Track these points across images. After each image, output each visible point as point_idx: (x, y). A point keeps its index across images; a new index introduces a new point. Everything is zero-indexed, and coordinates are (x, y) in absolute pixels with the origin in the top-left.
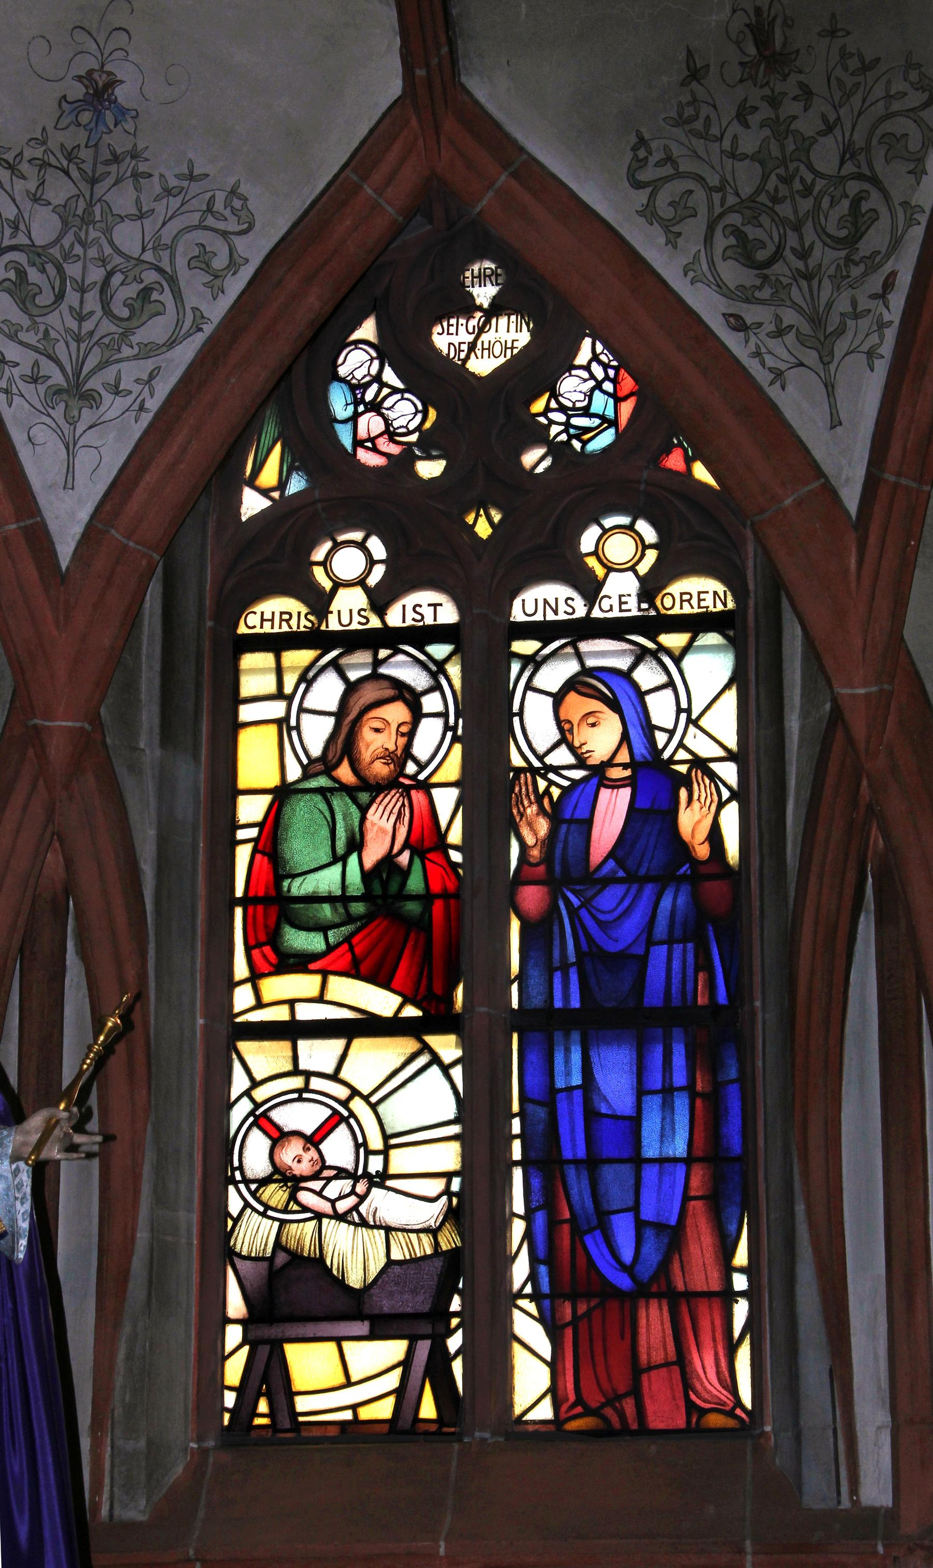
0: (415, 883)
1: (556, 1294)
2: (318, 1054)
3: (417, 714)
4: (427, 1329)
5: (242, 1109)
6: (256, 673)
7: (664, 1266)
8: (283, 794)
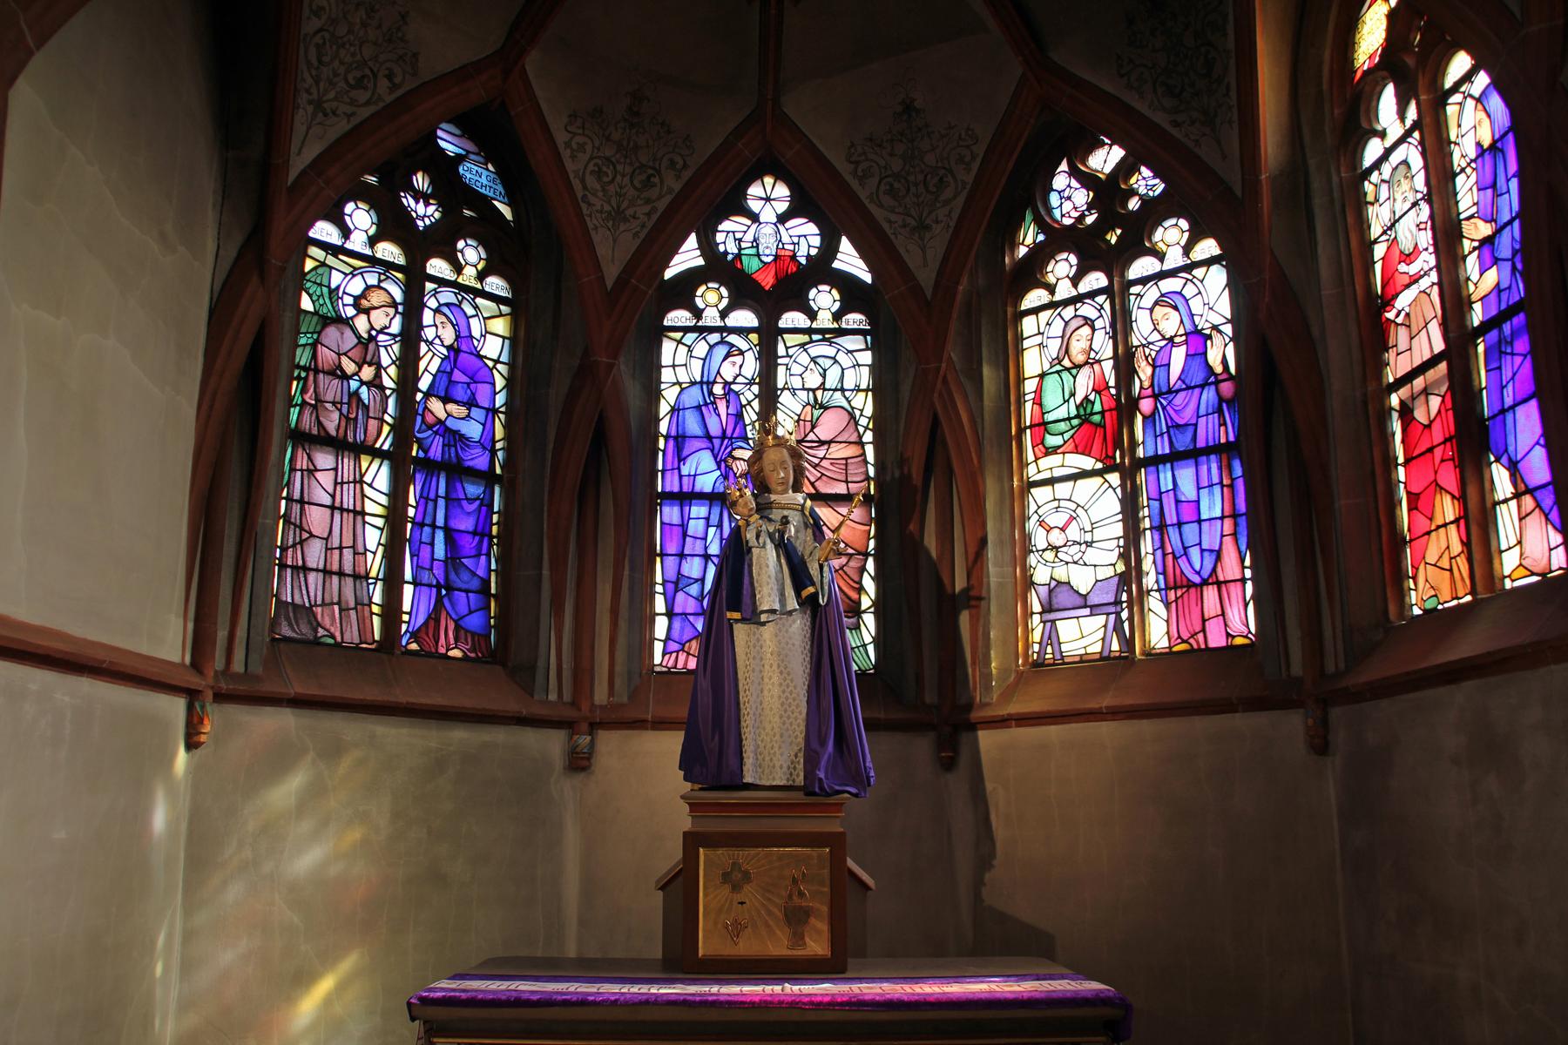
0: (1098, 407)
1: (1167, 588)
2: (1063, 489)
3: (1093, 330)
4: (1112, 609)
5: (1035, 518)
6: (1029, 325)
7: (1214, 570)
8: (1042, 376)
